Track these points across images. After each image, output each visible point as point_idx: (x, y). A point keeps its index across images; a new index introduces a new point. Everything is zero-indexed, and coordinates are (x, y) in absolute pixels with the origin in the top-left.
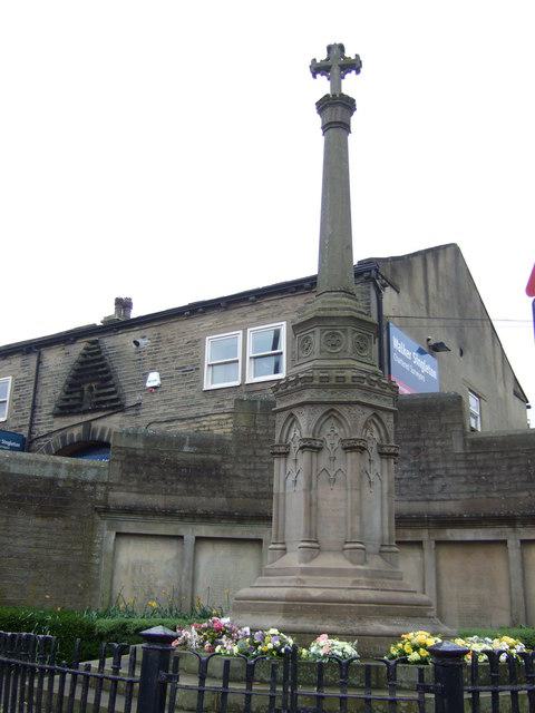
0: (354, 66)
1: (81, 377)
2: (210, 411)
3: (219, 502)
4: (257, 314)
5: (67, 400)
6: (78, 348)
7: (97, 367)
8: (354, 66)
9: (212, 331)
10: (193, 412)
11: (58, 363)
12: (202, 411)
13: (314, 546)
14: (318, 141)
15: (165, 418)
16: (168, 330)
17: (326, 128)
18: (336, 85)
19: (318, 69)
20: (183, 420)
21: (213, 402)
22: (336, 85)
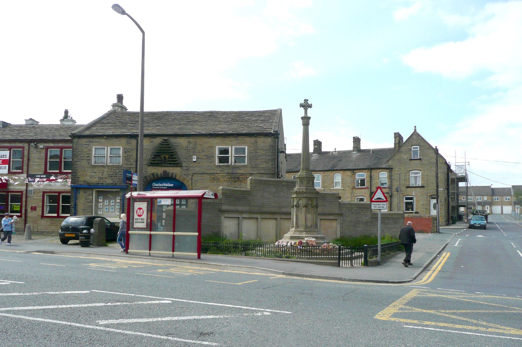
0: (310, 106)
1: (160, 153)
2: (219, 172)
3: (247, 208)
4: (236, 141)
5: (153, 161)
6: (159, 140)
7: (168, 150)
8: (310, 106)
9: (218, 144)
10: (211, 172)
11: (149, 146)
12: (215, 172)
13: (297, 226)
14: (302, 127)
15: (200, 172)
16: (199, 140)
17: (303, 125)
18: (306, 112)
19: (301, 105)
20: (207, 174)
21: (220, 169)
22: (306, 112)
